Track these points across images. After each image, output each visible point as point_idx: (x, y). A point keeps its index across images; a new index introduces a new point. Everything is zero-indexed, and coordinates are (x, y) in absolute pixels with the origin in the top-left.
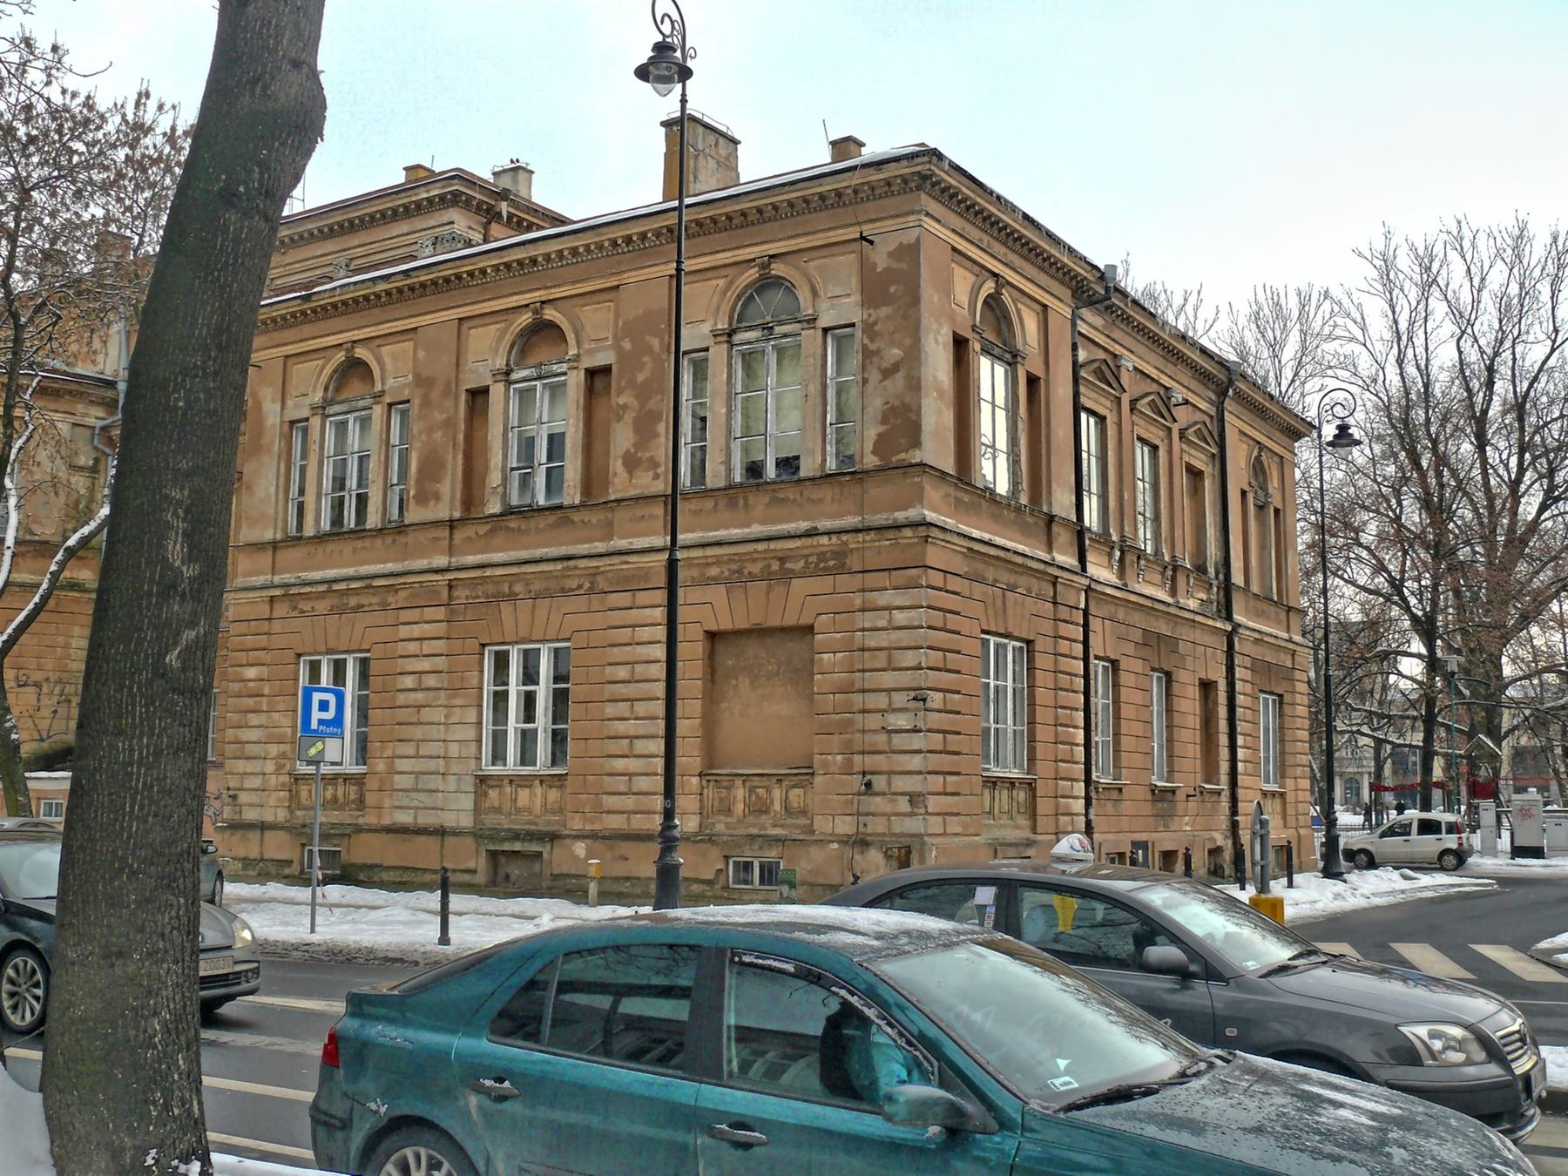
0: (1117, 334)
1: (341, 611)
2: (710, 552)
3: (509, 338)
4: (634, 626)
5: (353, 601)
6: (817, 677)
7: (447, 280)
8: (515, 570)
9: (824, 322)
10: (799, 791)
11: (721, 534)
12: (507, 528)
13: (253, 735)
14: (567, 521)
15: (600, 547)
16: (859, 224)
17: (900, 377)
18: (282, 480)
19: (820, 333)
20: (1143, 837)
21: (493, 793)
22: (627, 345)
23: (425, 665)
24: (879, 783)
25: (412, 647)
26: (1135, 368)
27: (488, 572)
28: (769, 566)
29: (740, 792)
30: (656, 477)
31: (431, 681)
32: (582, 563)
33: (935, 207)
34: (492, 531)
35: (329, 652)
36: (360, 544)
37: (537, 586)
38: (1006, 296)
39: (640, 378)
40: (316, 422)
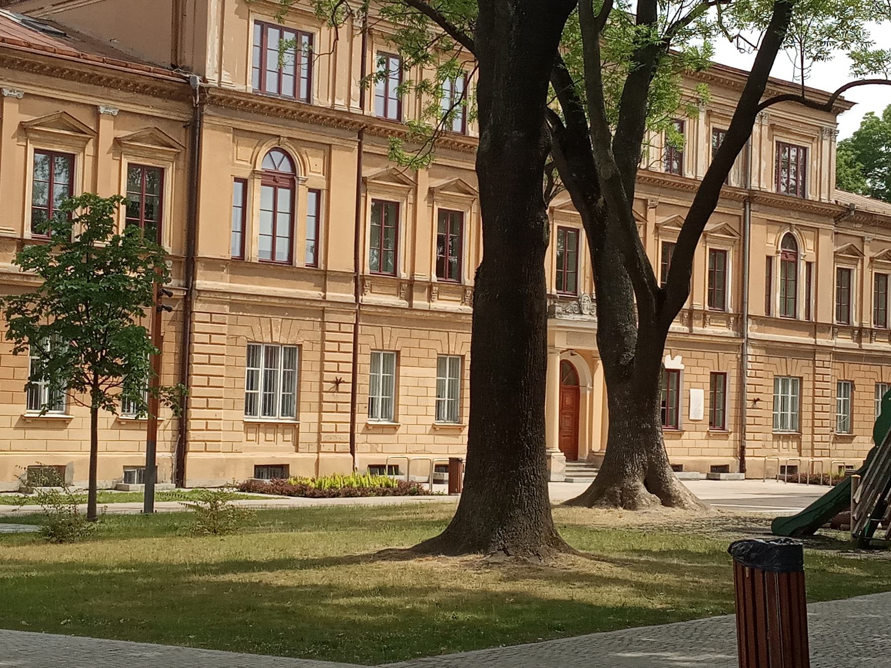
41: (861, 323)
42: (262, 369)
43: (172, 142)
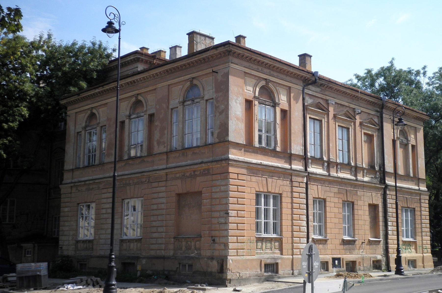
0: (327, 93)
2: (176, 169)
3: (130, 105)
4: (158, 193)
6: (202, 207)
9: (206, 98)
10: (198, 243)
11: (180, 164)
15: (151, 169)
16: (212, 67)
17: (224, 114)
18: (75, 150)
19: (205, 101)
20: (339, 256)
21: (124, 245)
22: (158, 107)
24: (217, 240)
26: (336, 103)
27: (123, 177)
28: (191, 173)
29: (184, 243)
30: (165, 147)
32: (145, 174)
33: (235, 60)
35: (86, 202)
37: (135, 181)
38: (271, 85)
39: (161, 117)
40: (83, 132)
41: (356, 163)
42: (263, 207)
43: (323, 108)
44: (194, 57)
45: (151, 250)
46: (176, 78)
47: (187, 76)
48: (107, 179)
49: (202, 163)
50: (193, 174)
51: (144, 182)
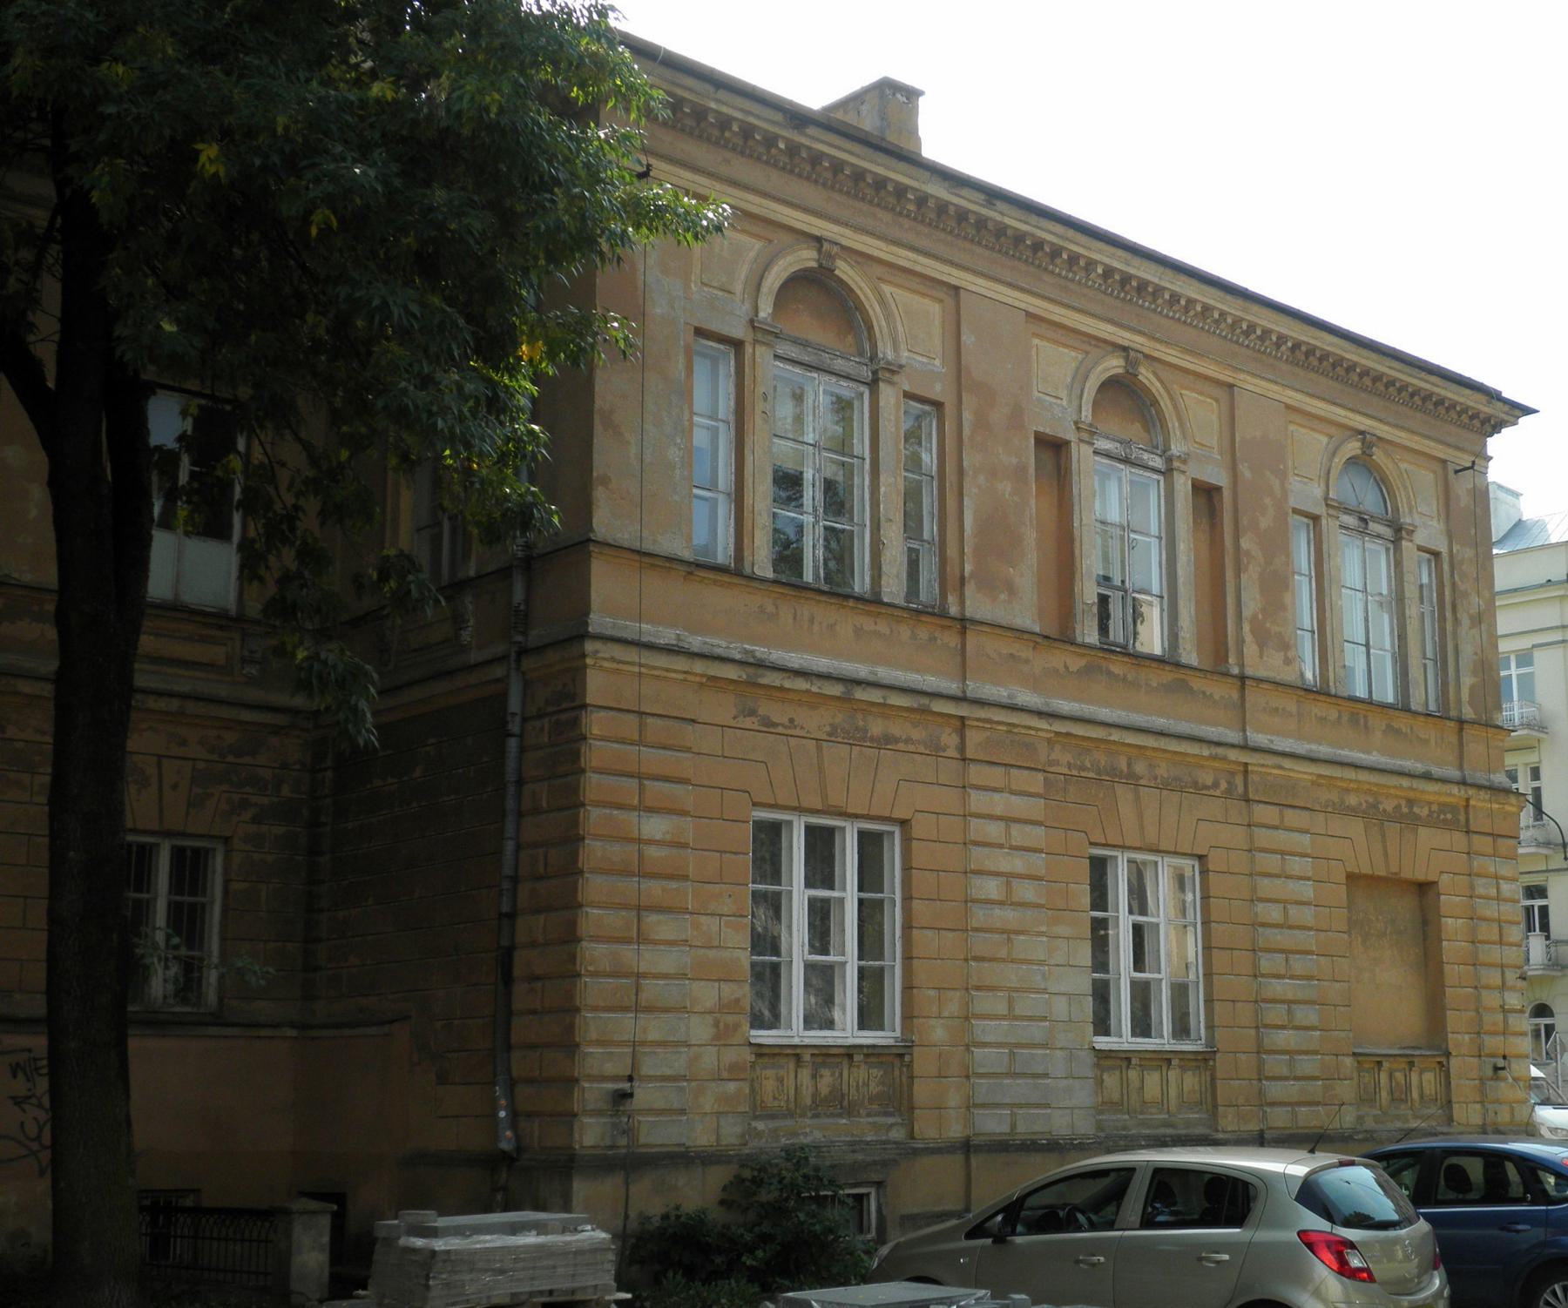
1: (857, 738)
5: (877, 727)
7: (1038, 246)
8: (1150, 742)
12: (1109, 673)
13: (666, 961)
14: (1182, 687)
23: (1017, 864)
25: (994, 830)
31: (1027, 891)
34: (1087, 671)
36: (868, 624)
37: (1163, 771)
44: (1423, 375)
45: (1273, 1104)
46: (1297, 390)
47: (1358, 418)
48: (1014, 718)
49: (1427, 777)
50: (1405, 810)
51: (1207, 787)
